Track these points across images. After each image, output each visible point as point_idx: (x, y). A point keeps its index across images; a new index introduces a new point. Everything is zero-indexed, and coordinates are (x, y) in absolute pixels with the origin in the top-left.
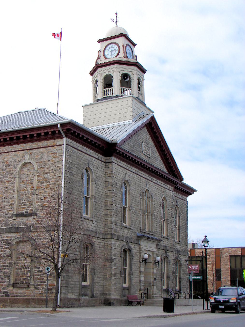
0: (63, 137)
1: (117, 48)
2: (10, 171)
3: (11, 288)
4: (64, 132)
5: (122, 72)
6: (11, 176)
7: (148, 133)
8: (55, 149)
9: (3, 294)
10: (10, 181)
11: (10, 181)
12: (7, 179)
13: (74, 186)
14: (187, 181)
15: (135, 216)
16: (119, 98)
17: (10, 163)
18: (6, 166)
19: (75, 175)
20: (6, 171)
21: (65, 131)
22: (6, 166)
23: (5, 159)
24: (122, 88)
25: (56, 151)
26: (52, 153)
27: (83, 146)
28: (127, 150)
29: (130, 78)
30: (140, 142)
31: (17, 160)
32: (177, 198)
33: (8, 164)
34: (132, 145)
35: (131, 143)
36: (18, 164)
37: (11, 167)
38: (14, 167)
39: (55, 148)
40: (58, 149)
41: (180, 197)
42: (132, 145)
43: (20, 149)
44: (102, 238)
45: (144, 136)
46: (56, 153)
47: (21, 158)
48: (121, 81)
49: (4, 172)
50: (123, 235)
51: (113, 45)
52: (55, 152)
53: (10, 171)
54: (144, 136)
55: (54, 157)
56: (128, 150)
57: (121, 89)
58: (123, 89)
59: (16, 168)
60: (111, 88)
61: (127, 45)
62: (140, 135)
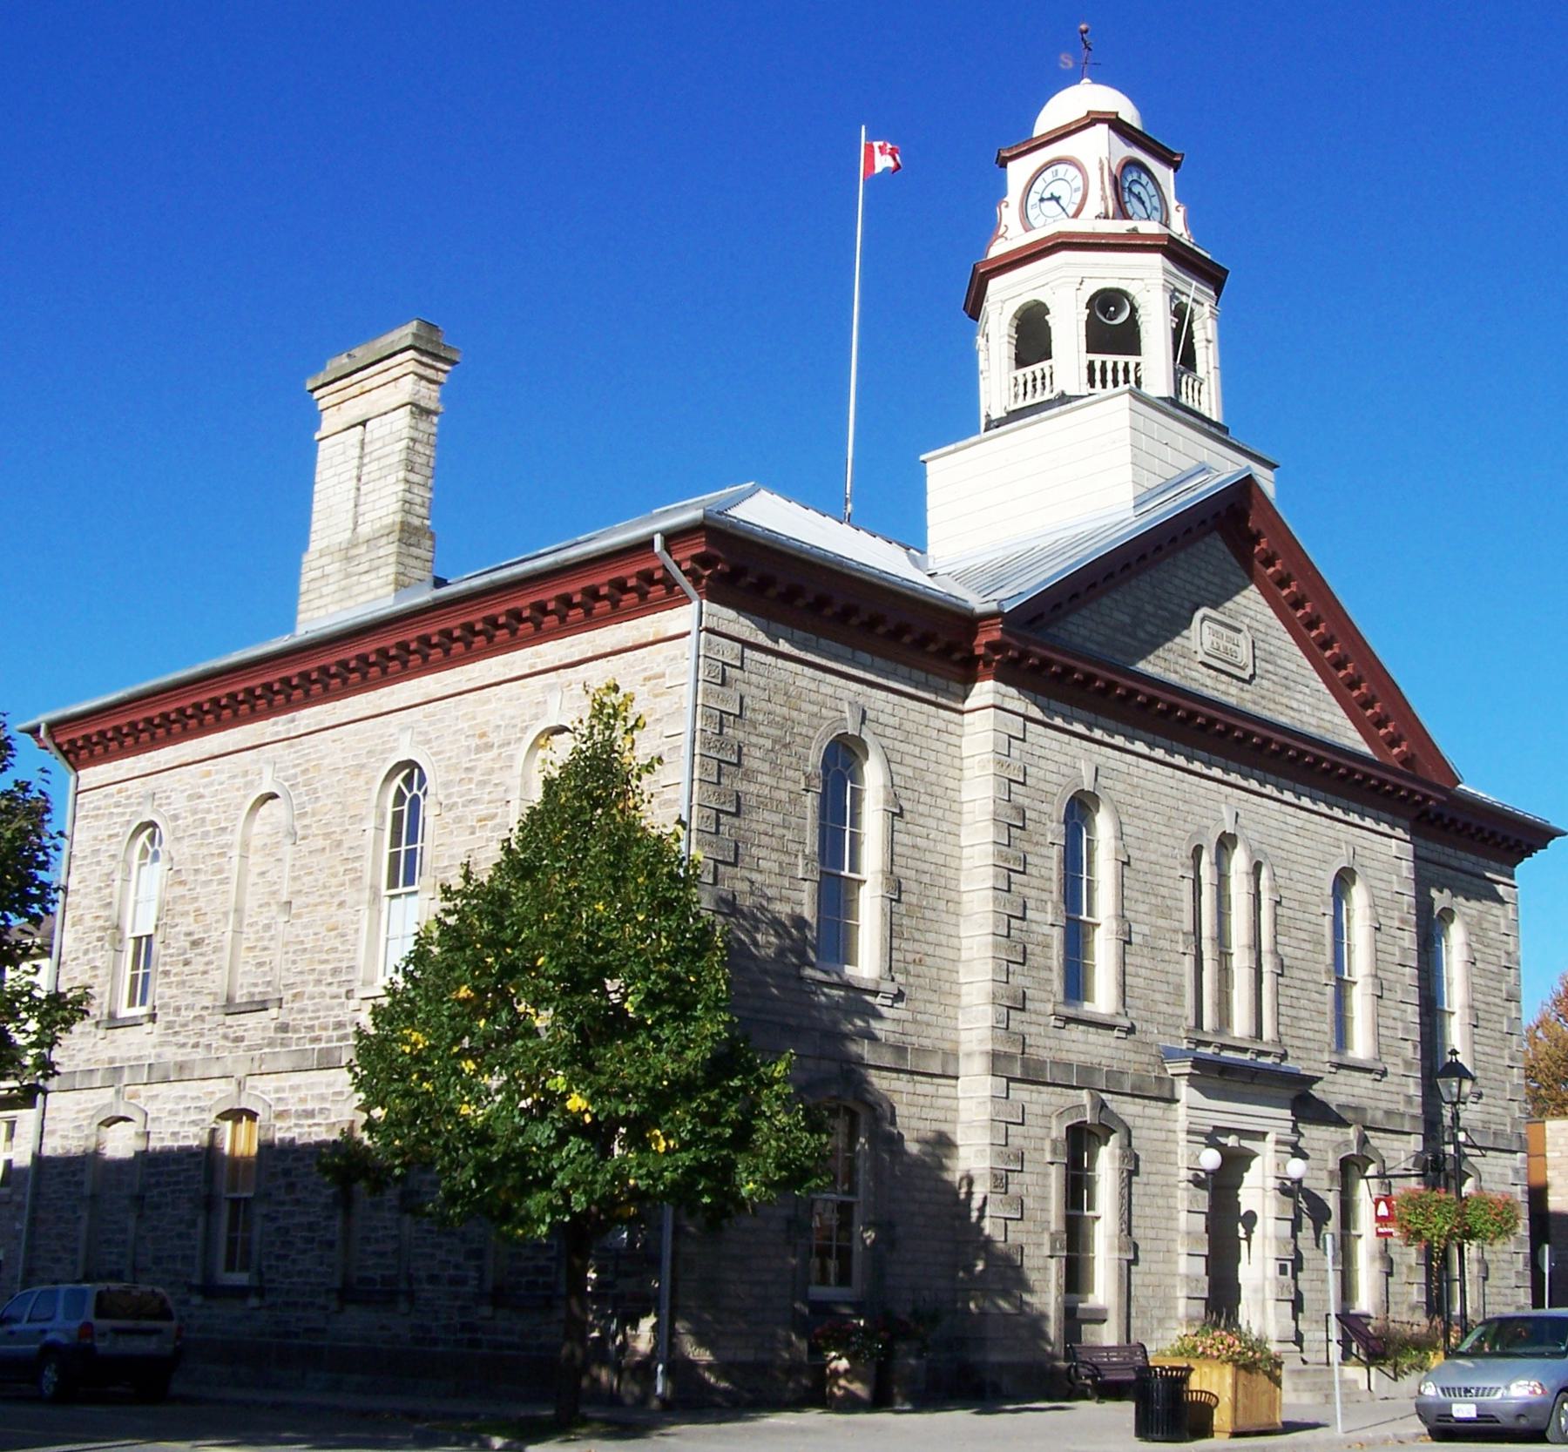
0: (687, 600)
1: (1079, 182)
2: (491, 771)
3: (486, 1311)
4: (685, 573)
5: (1091, 288)
6: (494, 796)
7: (1234, 561)
8: (660, 659)
9: (459, 1336)
10: (494, 816)
11: (494, 816)
12: (482, 809)
13: (754, 826)
14: (1481, 781)
15: (1146, 963)
16: (1074, 404)
17: (494, 738)
18: (478, 749)
19: (760, 778)
20: (477, 776)
21: (687, 566)
22: (478, 749)
23: (474, 718)
24: (1092, 357)
25: (663, 666)
26: (647, 674)
27: (303, 599)
28: (1089, 645)
29: (1134, 310)
30: (1182, 607)
31: (518, 721)
32: (1450, 872)
33: (485, 740)
34: (1127, 620)
35: (1117, 615)
36: (520, 739)
37: (495, 751)
38: (506, 751)
39: (659, 653)
40: (673, 653)
41: (1466, 865)
42: (1127, 620)
43: (531, 666)
44: (939, 1072)
45: (1211, 578)
46: (663, 675)
47: (534, 711)
48: (1091, 324)
49: (471, 780)
50: (1064, 1056)
51: (1061, 168)
52: (657, 670)
53: (491, 771)
54: (1211, 578)
55: (656, 696)
56: (1098, 644)
57: (1091, 366)
58: (1098, 366)
59: (511, 757)
60: (1045, 364)
61: (1131, 164)
62: (1180, 573)
